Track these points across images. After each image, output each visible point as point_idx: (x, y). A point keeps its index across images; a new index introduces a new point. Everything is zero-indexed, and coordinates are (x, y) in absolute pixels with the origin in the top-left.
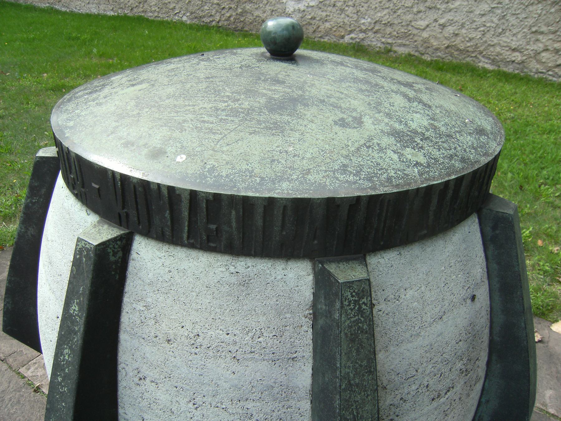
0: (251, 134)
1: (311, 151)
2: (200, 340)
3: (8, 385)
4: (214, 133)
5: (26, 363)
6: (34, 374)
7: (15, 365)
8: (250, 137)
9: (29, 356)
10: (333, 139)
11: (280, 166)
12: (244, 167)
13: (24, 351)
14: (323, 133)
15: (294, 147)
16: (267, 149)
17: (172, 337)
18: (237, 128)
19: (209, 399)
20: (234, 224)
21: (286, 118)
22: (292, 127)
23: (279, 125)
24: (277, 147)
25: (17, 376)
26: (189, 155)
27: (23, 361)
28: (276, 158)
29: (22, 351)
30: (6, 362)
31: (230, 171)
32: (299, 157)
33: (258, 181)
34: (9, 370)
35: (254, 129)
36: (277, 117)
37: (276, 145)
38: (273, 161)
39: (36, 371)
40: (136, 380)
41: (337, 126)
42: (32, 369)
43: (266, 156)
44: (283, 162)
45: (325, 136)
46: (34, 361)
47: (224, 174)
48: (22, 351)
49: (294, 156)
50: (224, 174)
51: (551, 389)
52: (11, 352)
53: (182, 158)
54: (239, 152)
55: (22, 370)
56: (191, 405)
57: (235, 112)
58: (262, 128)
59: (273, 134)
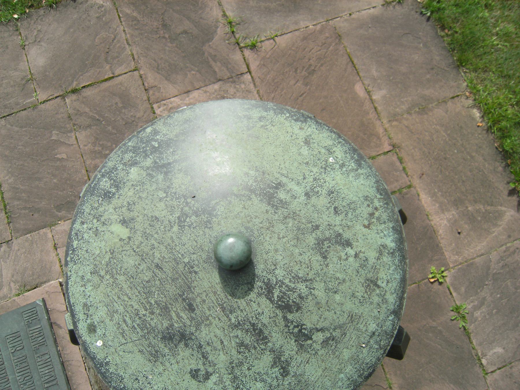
0: (139, 351)
1: (159, 386)
3: (143, 114)
4: (123, 336)
5: (159, 100)
6: (161, 114)
7: (152, 98)
8: (137, 353)
9: (164, 95)
10: (178, 384)
11: (138, 385)
12: (122, 373)
13: (162, 88)
14: (177, 376)
15: (153, 377)
16: (139, 369)
18: (136, 341)
21: (167, 351)
22: (163, 361)
23: (158, 354)
24: (145, 371)
25: (150, 109)
26: (104, 345)
27: (158, 98)
28: (139, 378)
29: (160, 88)
30: (148, 92)
31: (114, 371)
32: (150, 385)
33: (122, 387)
34: (147, 101)
35: (143, 348)
36: (162, 346)
37: (145, 369)
38: (137, 379)
39: (163, 112)
41: (189, 375)
42: (161, 109)
43: (136, 373)
44: (141, 384)
45: (176, 379)
46: (164, 102)
47: (111, 370)
48: (160, 88)
49: (149, 383)
50: (111, 370)
51: (504, 348)
52: (153, 85)
53: (100, 343)
54: (125, 361)
55: (155, 106)
57: (144, 325)
58: (147, 351)
59: (150, 360)
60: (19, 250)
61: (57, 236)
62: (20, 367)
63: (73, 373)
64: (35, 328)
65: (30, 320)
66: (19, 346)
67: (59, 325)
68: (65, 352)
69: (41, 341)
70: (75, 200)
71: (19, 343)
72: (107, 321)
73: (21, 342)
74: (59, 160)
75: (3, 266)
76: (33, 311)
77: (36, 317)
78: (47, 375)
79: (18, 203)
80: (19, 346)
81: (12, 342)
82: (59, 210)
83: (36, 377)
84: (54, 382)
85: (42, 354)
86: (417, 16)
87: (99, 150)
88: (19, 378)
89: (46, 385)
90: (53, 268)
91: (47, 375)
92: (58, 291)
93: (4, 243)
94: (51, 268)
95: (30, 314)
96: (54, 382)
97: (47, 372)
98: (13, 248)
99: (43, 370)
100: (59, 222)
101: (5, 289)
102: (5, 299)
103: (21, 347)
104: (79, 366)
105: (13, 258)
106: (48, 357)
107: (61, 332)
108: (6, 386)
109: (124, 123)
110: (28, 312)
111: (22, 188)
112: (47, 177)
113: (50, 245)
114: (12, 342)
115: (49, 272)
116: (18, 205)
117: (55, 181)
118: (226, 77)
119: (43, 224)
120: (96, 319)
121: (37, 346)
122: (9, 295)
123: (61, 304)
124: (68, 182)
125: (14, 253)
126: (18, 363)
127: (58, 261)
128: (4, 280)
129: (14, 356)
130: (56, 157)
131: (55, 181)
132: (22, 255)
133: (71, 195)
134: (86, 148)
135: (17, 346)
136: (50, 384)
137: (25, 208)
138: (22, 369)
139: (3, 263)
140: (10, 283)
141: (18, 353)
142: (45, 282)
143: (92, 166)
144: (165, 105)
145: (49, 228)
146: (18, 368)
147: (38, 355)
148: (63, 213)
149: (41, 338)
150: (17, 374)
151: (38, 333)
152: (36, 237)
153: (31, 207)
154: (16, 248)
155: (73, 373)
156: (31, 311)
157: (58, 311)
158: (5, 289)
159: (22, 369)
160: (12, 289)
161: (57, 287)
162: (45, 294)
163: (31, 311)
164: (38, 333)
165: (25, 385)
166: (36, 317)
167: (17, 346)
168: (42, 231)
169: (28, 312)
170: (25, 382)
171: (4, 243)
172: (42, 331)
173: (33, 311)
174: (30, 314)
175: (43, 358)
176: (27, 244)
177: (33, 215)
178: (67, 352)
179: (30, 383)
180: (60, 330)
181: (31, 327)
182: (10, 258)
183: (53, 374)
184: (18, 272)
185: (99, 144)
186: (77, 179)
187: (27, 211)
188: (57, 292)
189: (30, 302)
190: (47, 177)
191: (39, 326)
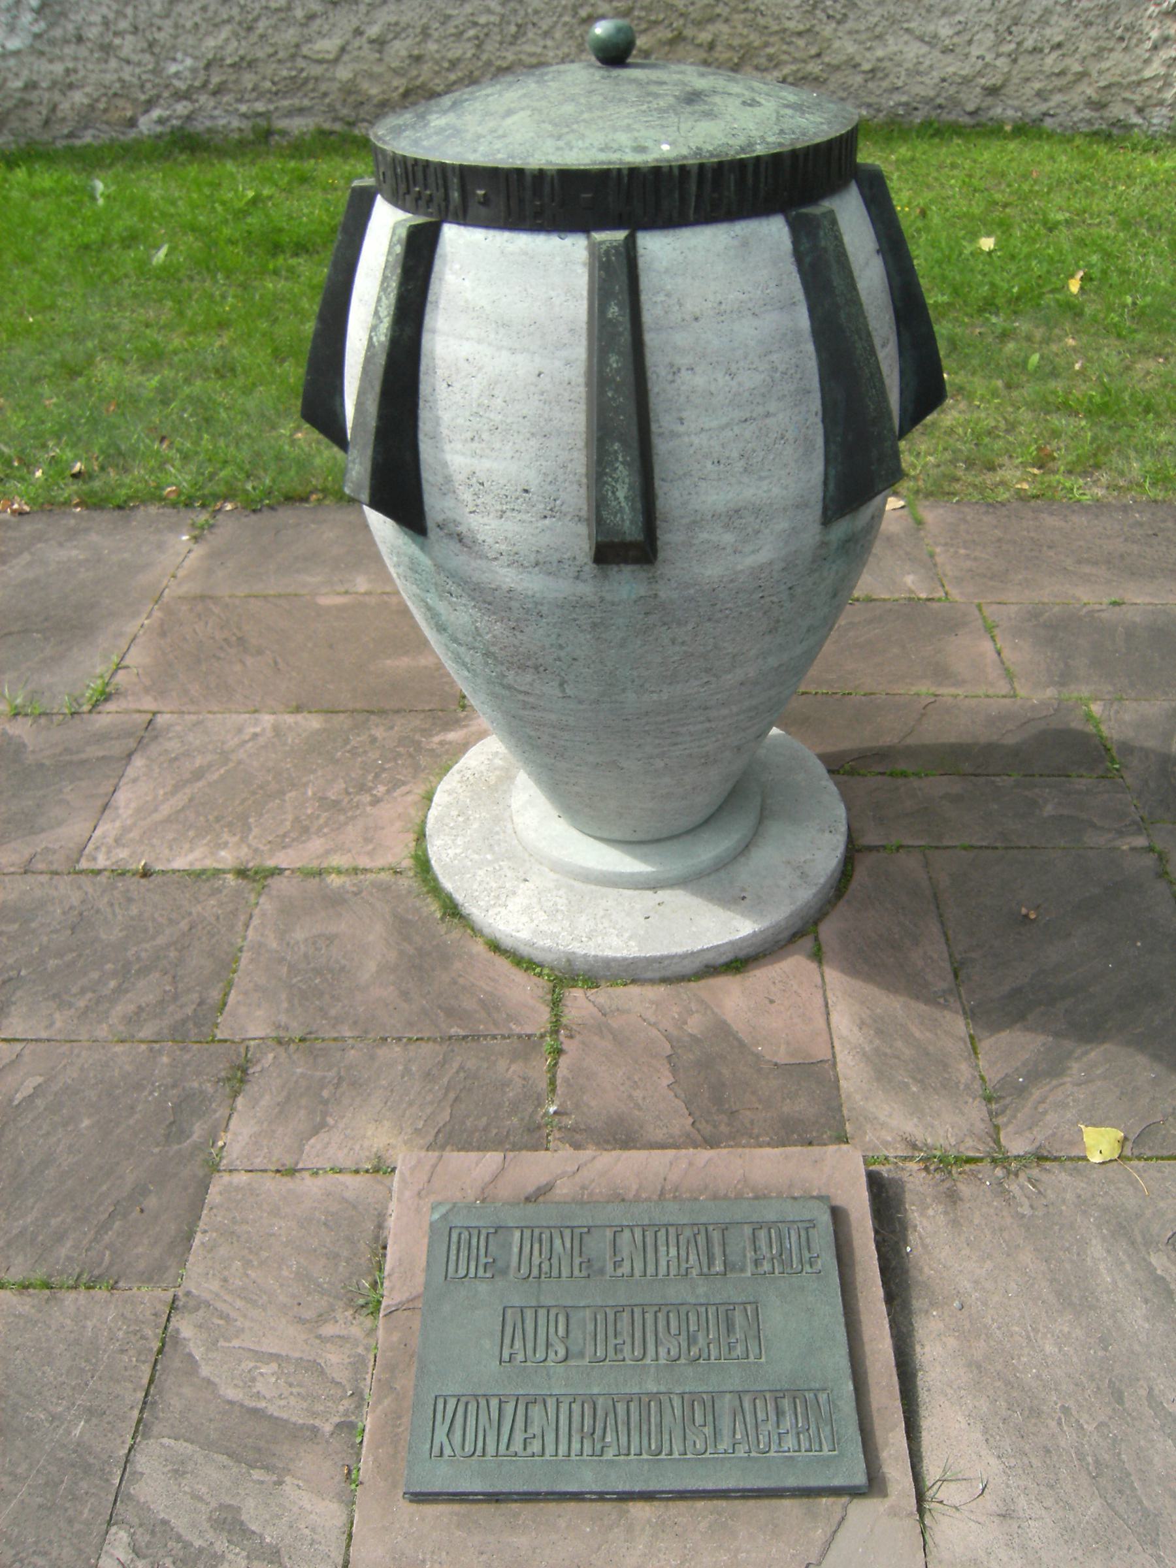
2: (723, 307)
17: (698, 314)
19: (742, 364)
20: (732, 188)
40: (670, 377)
46: (90, 846)
56: (728, 378)
60: (225, 1280)
61: (258, 1160)
62: (628, 1341)
63: (706, 1187)
64: (516, 1250)
65: (483, 1260)
66: (552, 1324)
67: (539, 1189)
68: (633, 1193)
69: (568, 1245)
70: (184, 1089)
71: (542, 1321)
72: (636, 134)
73: (542, 1313)
74: (30, 1098)
75: (244, 1345)
76: (459, 1242)
77: (482, 1238)
78: (683, 1253)
79: (69, 1244)
80: (552, 1324)
81: (530, 1345)
82: (183, 1134)
83: (676, 1292)
84: (716, 1236)
85: (609, 1252)
86: (254, 517)
87: (90, 1000)
88: (662, 1352)
89: (718, 1267)
90: (347, 1194)
91: (683, 1253)
92: (433, 1161)
93: (168, 1320)
94: (344, 1200)
95: (463, 1254)
96: (716, 1236)
97: (673, 1252)
98: (206, 1296)
99: (663, 1263)
100: (220, 1143)
101: (329, 1356)
102: (366, 1366)
103: (562, 1319)
104: (690, 1164)
105: (239, 1303)
106: (627, 1233)
107: (565, 1191)
108: (678, 1413)
109: (69, 932)
110: (453, 1257)
111: (29, 1220)
112: (59, 1140)
113: (271, 1185)
114: (530, 1345)
115: (355, 1207)
116: (76, 1247)
117: (86, 1122)
118: (395, 95)
119: (191, 1191)
120: (630, 143)
121: (577, 1261)
122: (360, 1350)
123: (477, 1164)
124: (118, 1091)
125: (227, 1298)
126: (612, 1342)
127: (337, 1176)
128: (297, 1355)
129: (581, 1355)
130: (16, 1102)
131: (86, 1122)
132: (247, 1276)
133: (160, 1095)
134: (58, 1025)
135: (552, 1330)
136: (717, 1250)
137: (104, 1227)
138: (638, 1335)
139: (236, 1343)
140: (319, 1337)
141: (576, 1333)
142: (380, 1226)
143: (121, 1028)
144: (97, 848)
145: (217, 1175)
146: (627, 1349)
147: (609, 1267)
148: (198, 1131)
149: (557, 1242)
150: (648, 1361)
151: (536, 1246)
152: (219, 1219)
153: (112, 1209)
154: (215, 1285)
155: (706, 1187)
156: (454, 1247)
157: (495, 1178)
158: (329, 1356)
159: (638, 1335)
160: (344, 1333)
161: (419, 1162)
162: (421, 1202)
163: (454, 1247)
164: (536, 1246)
165: (695, 1342)
166: (482, 1238)
167: (552, 1330)
168: (214, 1194)
169: (453, 1257)
170: (683, 1339)
171: (168, 1320)
172: (537, 1232)
173: (459, 1242)
174: (463, 1254)
175: (625, 1253)
176: (223, 1251)
177: (142, 1211)
178: (635, 1187)
179: (693, 1318)
180: (558, 1191)
181: (508, 1267)
182: (233, 1314)
183: (688, 1232)
184: (296, 1302)
185: (75, 995)
186: (128, 1068)
187: (117, 1225)
188: (435, 1166)
189: (424, 1258)
190: (59, 1140)
191: (517, 1234)
